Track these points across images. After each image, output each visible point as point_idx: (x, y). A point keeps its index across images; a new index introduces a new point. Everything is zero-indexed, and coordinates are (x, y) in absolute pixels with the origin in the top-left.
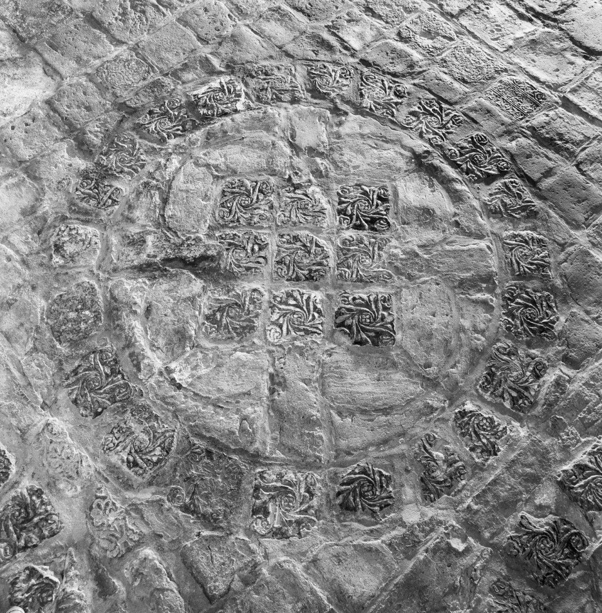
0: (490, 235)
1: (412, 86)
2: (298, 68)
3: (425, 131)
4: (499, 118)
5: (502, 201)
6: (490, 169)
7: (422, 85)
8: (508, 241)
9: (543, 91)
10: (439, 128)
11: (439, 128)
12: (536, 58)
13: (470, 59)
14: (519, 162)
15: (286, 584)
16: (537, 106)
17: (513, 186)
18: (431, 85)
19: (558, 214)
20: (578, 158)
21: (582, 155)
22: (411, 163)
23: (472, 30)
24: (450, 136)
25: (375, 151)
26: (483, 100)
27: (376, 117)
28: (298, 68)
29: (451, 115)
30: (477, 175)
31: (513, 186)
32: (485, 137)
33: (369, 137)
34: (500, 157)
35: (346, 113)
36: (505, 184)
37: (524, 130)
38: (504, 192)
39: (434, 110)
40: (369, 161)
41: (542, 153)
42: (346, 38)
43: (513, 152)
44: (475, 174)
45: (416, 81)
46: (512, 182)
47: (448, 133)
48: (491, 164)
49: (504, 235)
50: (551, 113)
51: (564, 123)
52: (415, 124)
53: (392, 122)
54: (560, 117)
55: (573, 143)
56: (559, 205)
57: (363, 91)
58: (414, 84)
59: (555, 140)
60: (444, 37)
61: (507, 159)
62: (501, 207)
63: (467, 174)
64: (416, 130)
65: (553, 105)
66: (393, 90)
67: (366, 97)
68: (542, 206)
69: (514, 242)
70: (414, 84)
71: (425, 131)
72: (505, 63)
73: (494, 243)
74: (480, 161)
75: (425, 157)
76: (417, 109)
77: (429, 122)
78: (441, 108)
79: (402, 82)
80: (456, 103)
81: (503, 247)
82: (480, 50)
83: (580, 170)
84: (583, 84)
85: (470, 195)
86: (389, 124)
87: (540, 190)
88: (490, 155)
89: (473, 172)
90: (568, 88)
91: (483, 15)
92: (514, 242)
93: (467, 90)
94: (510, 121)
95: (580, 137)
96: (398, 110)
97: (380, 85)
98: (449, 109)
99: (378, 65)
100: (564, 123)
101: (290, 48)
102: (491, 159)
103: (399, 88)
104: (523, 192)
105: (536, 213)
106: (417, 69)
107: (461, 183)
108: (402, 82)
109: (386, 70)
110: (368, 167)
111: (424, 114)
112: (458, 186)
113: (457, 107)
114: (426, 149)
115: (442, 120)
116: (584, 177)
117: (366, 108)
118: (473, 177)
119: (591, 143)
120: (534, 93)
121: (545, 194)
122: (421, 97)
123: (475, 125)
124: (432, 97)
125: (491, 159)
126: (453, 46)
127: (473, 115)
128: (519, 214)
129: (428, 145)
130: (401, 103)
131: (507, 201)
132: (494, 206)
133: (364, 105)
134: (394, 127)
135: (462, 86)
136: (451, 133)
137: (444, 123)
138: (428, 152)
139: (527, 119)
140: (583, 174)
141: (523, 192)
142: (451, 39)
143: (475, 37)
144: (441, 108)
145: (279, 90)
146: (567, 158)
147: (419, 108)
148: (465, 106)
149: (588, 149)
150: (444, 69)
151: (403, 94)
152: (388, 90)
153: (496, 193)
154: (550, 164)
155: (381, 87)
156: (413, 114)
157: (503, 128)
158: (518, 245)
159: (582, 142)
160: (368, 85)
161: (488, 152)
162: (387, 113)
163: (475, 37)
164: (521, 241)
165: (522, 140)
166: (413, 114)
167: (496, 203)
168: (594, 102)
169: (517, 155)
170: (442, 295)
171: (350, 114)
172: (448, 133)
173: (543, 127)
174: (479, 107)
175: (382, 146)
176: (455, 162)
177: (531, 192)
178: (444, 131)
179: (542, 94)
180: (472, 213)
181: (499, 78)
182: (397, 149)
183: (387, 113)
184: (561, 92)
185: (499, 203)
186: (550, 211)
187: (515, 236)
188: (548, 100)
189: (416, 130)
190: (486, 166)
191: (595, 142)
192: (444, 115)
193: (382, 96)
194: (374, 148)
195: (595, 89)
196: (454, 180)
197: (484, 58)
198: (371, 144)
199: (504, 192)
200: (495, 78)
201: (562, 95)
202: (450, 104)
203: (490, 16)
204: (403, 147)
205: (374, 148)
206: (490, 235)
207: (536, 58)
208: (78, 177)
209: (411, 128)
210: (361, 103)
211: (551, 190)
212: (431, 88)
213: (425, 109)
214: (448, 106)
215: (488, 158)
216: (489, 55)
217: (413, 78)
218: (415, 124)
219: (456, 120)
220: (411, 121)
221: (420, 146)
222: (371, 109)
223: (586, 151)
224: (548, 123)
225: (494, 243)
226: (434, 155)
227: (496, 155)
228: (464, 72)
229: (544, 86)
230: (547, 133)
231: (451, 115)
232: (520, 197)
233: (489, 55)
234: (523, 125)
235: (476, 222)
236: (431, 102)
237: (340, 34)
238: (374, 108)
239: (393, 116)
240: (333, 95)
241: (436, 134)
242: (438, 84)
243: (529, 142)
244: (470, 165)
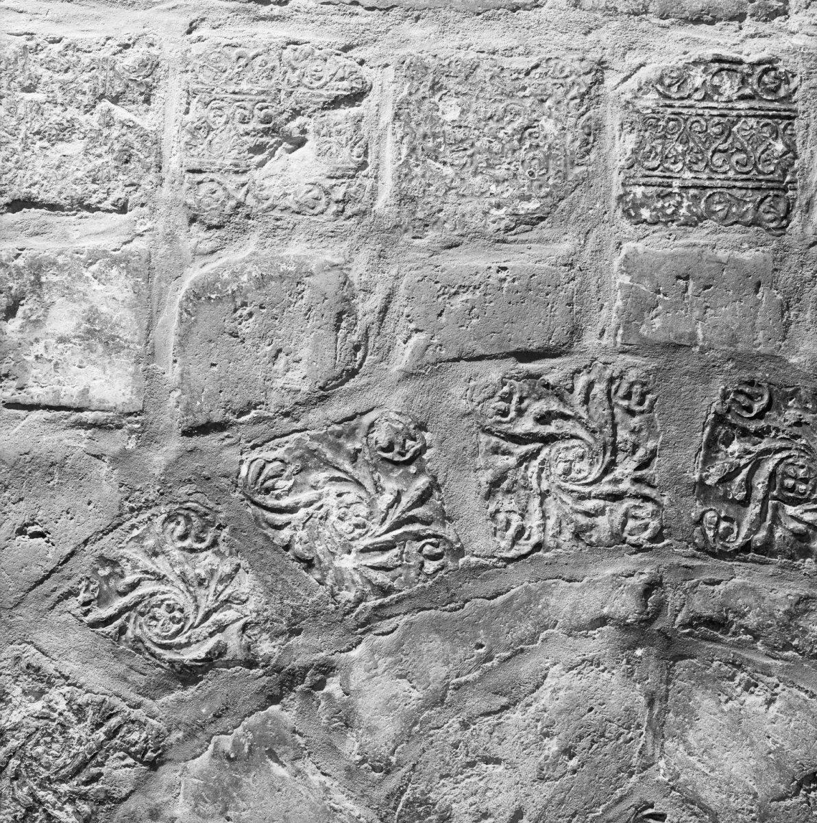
2: (44, 638)
10: (606, 471)
11: (606, 471)
25: (515, 717)
28: (44, 638)
39: (543, 419)
40: (529, 767)
42: (70, 394)
80: (576, 332)
93: (565, 247)
99: (251, 406)
101: (190, 492)
109: (288, 402)
110: (546, 789)
113: (590, 340)
145: (77, 771)
160: (292, 510)
170: (372, 36)
194: (505, 708)
198: (484, 706)
205: (505, 708)
208: (346, 737)
220: (516, 520)
231: (599, 389)
237: (36, 393)
240: (233, 641)
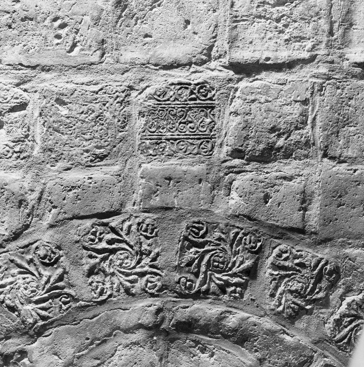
0: (315, 348)
1: (51, 232)
3: (128, 284)
4: (188, 177)
5: (291, 292)
6: (242, 263)
7: (60, 217)
8: (338, 337)
9: (198, 78)
11: (139, 262)
12: (145, 28)
13: (74, 113)
14: (263, 218)
15: (292, 101)
16: (213, 108)
17: (286, 259)
18: (71, 208)
19: (358, 247)
20: (318, 142)
21: (319, 135)
22: (155, 342)
23: (34, 61)
24: (159, 262)
26: (149, 166)
27: (60, 322)
29: (134, 228)
30: (236, 285)
31: (286, 259)
32: (198, 223)
33: (79, 358)
34: (237, 233)
35: (23, 353)
36: (275, 266)
37: (228, 164)
38: (282, 277)
39: (110, 242)
41: (277, 178)
43: (246, 212)
44: (232, 285)
45: (49, 218)
46: (279, 256)
47: (154, 259)
48: (237, 253)
49: (328, 333)
50: (237, 104)
51: (264, 107)
52: (108, 285)
53: (82, 308)
54: (253, 101)
55: (297, 128)
56: (350, 233)
57: (8, 302)
58: (52, 226)
59: (274, 143)
60: (13, 110)
61: (246, 225)
62: (295, 300)
63: (224, 292)
64: (118, 291)
65: (230, 89)
66: (37, 261)
67: (20, 306)
68: (334, 254)
69: (347, 330)
70: (52, 226)
71: (128, 284)
72: (119, 77)
73: (327, 353)
74: (223, 263)
75: (163, 319)
76: (93, 261)
77: (121, 265)
78: (113, 230)
79: (35, 237)
80: (122, 205)
81: (339, 348)
82: (71, 86)
83: (332, 158)
84: (235, 19)
85: (254, 319)
86: (81, 315)
87: (315, 233)
88: (224, 241)
89: (228, 284)
90: (222, 44)
91: (23, 20)
92: (347, 330)
93: (117, 168)
94: (203, 166)
95: (297, 109)
96: (71, 286)
97: (16, 271)
98: (124, 221)
100: (264, 107)
102: (231, 246)
103: (42, 252)
104: (301, 256)
105: (336, 271)
106: (32, 198)
107: (230, 312)
108: (35, 237)
111: (104, 259)
112: (232, 321)
113: (129, 207)
114: (153, 309)
115: (131, 247)
116: (344, 165)
117: (36, 322)
118: (234, 291)
119: (313, 104)
120: (192, 93)
121: (324, 235)
122: (77, 238)
123: (171, 215)
124: (88, 223)
125: (231, 246)
126: (37, 114)
127: (156, 201)
128: (320, 289)
129: (149, 301)
130: (65, 272)
131: (296, 286)
132: (289, 307)
133: (31, 321)
134: (91, 314)
135: (105, 169)
136: (158, 254)
137: (136, 248)
138: (159, 311)
139: (219, 141)
140: (341, 162)
141: (301, 256)
142: (23, 106)
143: (46, 69)
144: (113, 230)
146: (306, 156)
147: (91, 257)
148: (137, 197)
149: (318, 118)
150: (60, 165)
151: (54, 257)
152: (32, 269)
153: (276, 288)
154: (296, 185)
155: (21, 273)
156: (91, 272)
157: (205, 186)
158: (352, 330)
159: (304, 114)
161: (220, 239)
162: (65, 303)
163: (46, 69)
164: (351, 322)
165: (240, 181)
166: (91, 272)
167: (286, 301)
168: (269, 35)
169: (254, 210)
171: (28, 348)
172: (154, 259)
173: (246, 138)
174: (152, 184)
175: (104, 354)
176: (199, 292)
177: (309, 246)
178: (146, 260)
179: (202, 85)
180: (275, 342)
181: (134, 110)
182: (124, 342)
183: (65, 303)
184: (220, 57)
185: (290, 297)
186: (348, 251)
187: (338, 322)
188: (217, 86)
189: (118, 291)
190: (234, 263)
191: (318, 98)
192: (126, 238)
193: (34, 284)
195: (254, 11)
196: (221, 317)
197: (90, 97)
199: (282, 277)
200: (130, 116)
201: (225, 61)
202: (116, 213)
203: (31, 12)
204: (128, 331)
206: (315, 348)
207: (145, 28)
209: (110, 296)
210: (23, 322)
211: (326, 221)
212: (76, 212)
213: (99, 251)
214: (119, 219)
215: (227, 247)
216: (89, 84)
217: (40, 217)
218: (108, 285)
219: (146, 231)
220: (101, 286)
221: (143, 310)
222: (43, 318)
223: (319, 124)
224: (247, 126)
225: (327, 353)
226: (169, 306)
227: (232, 235)
228: (89, 145)
229: (194, 68)
230: (258, 142)
231: (134, 228)
232: (302, 265)
233: (89, 84)
234: (223, 156)
235: (288, 348)
236: (94, 234)
238: (43, 313)
239: (77, 300)
241: (142, 275)
242: (77, 198)
243: (249, 176)
244: (219, 278)
